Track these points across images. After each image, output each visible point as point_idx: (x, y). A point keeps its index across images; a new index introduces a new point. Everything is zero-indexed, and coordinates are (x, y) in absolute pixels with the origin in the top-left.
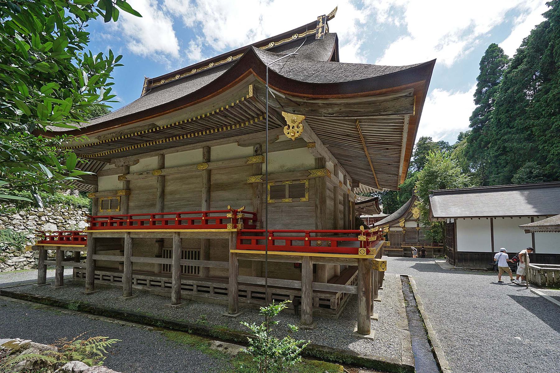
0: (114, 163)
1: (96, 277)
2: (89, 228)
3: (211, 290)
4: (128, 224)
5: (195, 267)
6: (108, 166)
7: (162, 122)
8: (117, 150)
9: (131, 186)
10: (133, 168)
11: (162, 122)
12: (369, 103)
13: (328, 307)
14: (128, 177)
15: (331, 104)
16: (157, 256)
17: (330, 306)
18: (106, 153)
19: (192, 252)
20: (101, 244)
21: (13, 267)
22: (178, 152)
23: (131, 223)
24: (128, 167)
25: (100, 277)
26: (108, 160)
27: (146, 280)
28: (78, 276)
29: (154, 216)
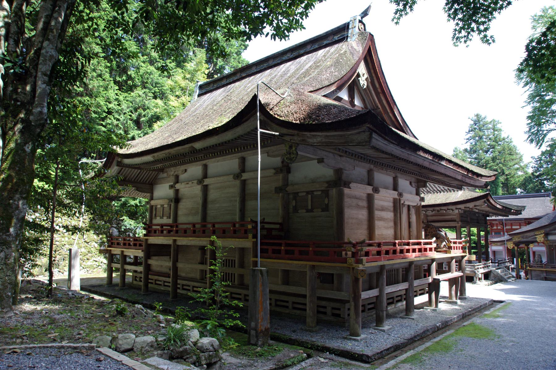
0: (166, 172)
1: (150, 281)
2: (145, 235)
3: (290, 305)
4: (175, 231)
5: (232, 274)
6: (162, 175)
7: (198, 145)
8: (167, 164)
9: (180, 195)
10: (182, 177)
11: (198, 145)
12: (341, 136)
13: (338, 315)
14: (178, 186)
15: (316, 135)
16: (200, 263)
17: (340, 315)
18: (159, 166)
19: (229, 260)
20: (152, 251)
21: (86, 270)
22: (218, 162)
23: (177, 232)
24: (177, 177)
25: (290, 305)
26: (162, 170)
27: (240, 294)
28: (136, 280)
29: (194, 225)
